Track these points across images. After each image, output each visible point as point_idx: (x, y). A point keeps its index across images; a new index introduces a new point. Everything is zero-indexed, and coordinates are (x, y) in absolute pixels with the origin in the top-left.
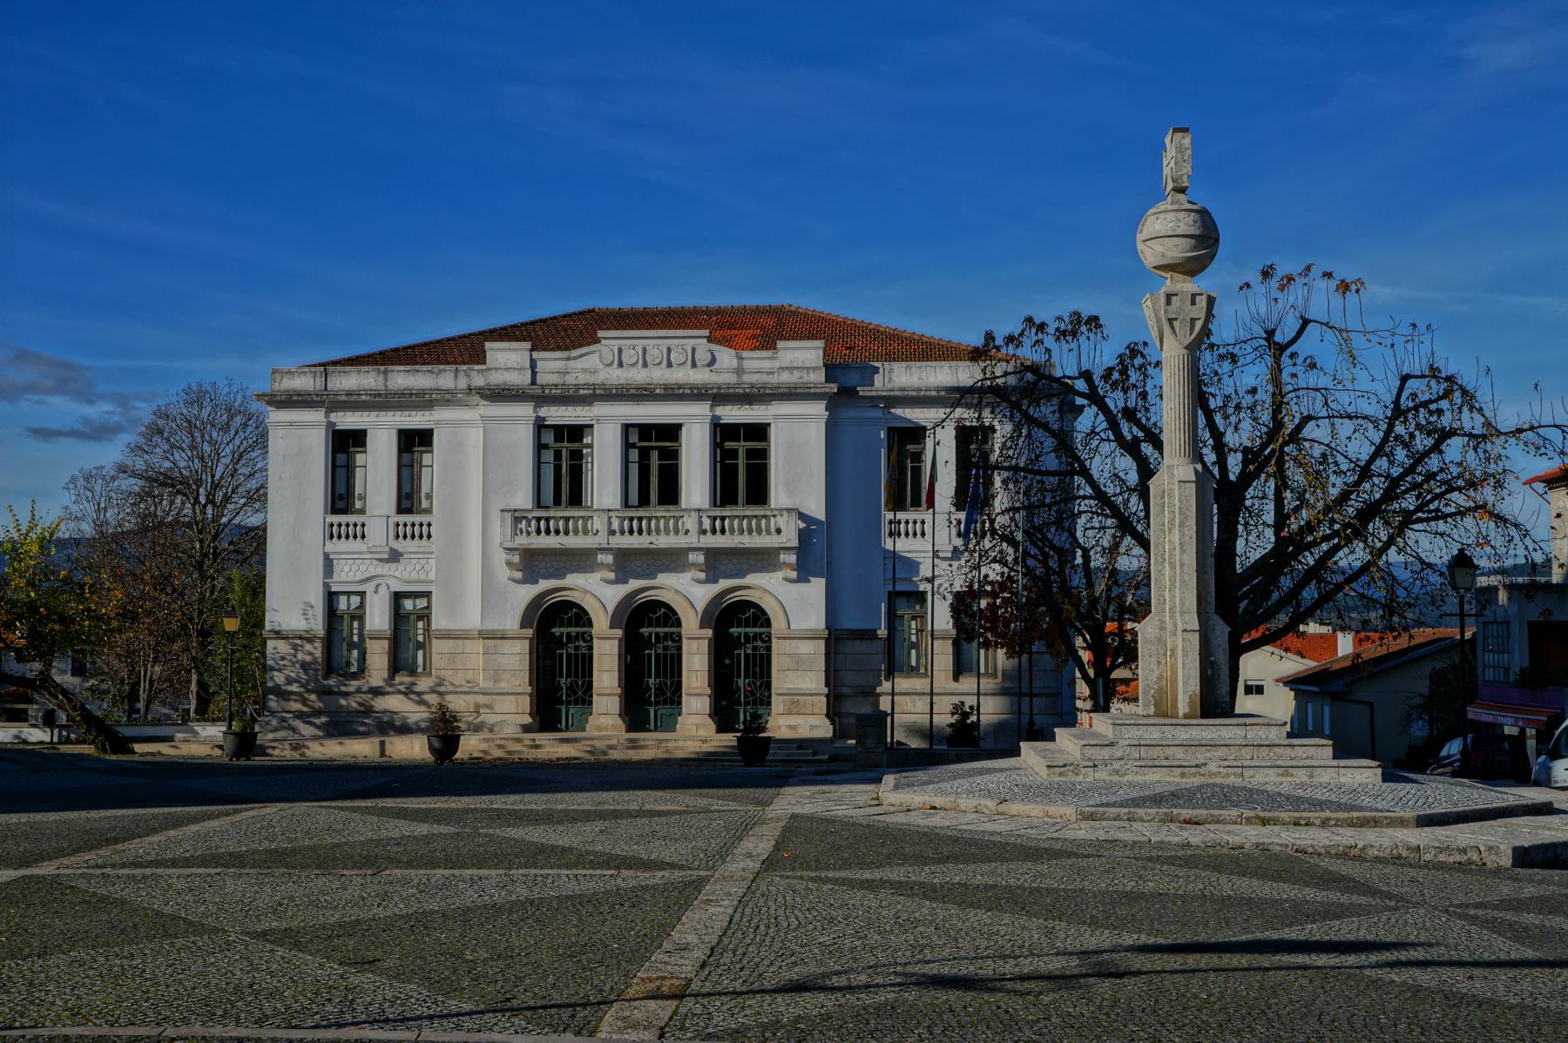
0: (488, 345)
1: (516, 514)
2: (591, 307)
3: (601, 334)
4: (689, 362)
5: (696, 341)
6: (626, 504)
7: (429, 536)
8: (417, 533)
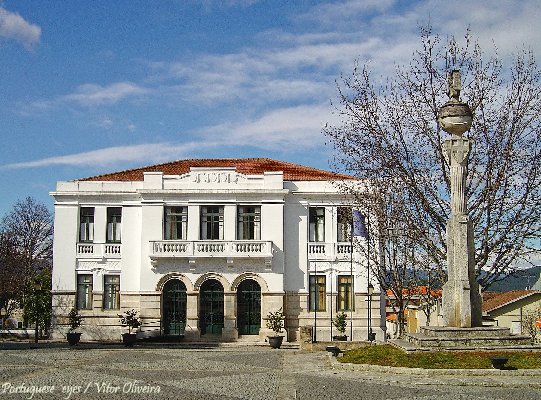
0: (145, 173)
1: (156, 243)
2: (186, 159)
3: (191, 168)
4: (227, 180)
5: (231, 173)
6: (201, 238)
7: (119, 252)
8: (114, 250)
